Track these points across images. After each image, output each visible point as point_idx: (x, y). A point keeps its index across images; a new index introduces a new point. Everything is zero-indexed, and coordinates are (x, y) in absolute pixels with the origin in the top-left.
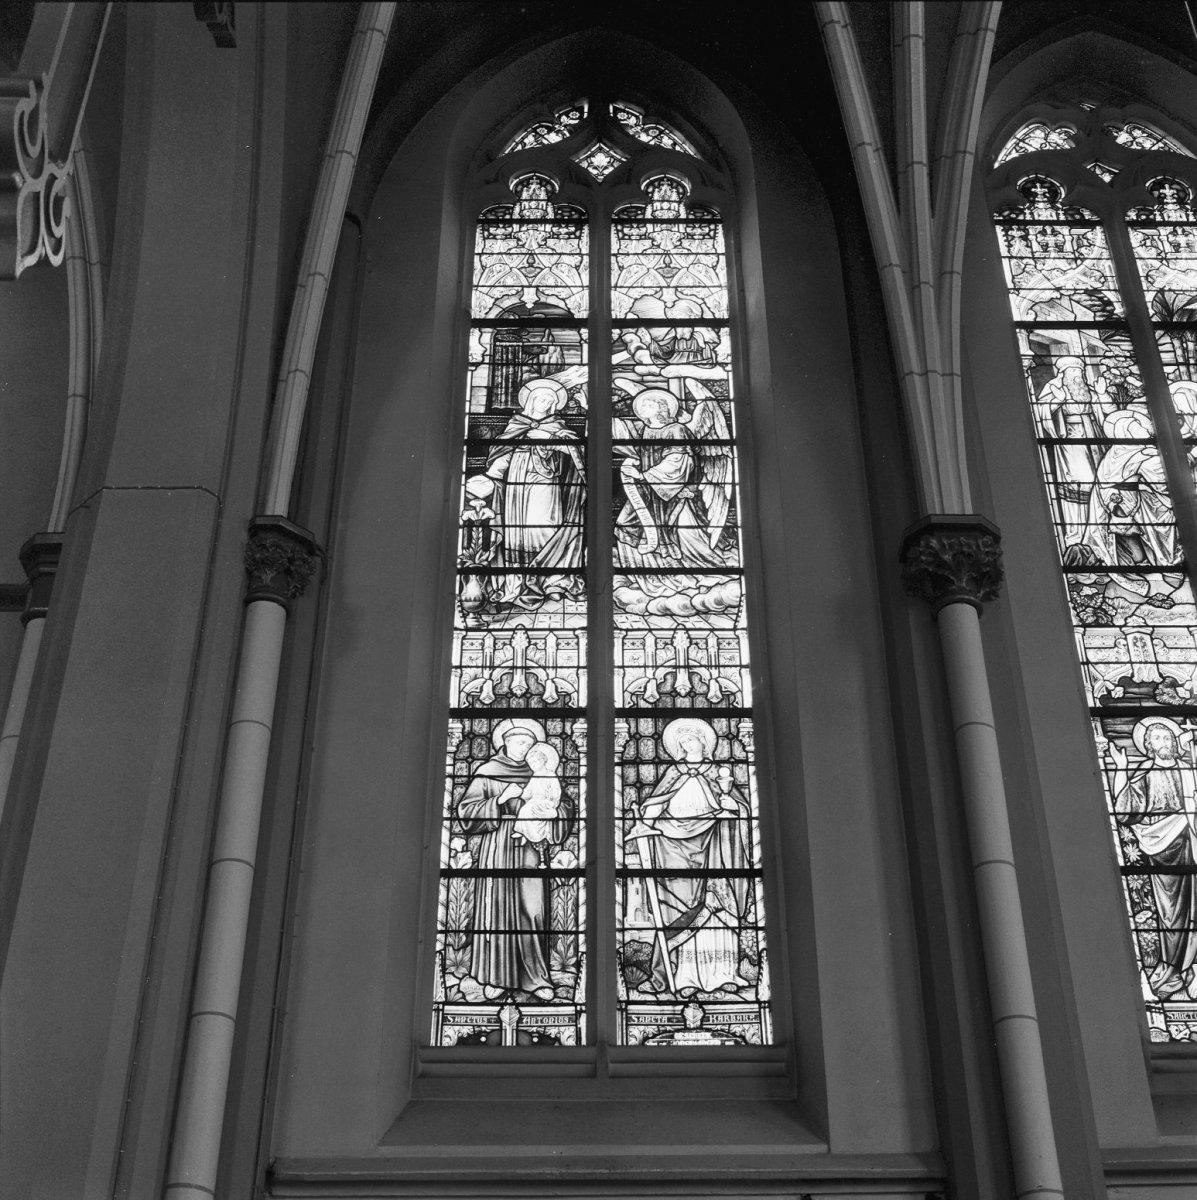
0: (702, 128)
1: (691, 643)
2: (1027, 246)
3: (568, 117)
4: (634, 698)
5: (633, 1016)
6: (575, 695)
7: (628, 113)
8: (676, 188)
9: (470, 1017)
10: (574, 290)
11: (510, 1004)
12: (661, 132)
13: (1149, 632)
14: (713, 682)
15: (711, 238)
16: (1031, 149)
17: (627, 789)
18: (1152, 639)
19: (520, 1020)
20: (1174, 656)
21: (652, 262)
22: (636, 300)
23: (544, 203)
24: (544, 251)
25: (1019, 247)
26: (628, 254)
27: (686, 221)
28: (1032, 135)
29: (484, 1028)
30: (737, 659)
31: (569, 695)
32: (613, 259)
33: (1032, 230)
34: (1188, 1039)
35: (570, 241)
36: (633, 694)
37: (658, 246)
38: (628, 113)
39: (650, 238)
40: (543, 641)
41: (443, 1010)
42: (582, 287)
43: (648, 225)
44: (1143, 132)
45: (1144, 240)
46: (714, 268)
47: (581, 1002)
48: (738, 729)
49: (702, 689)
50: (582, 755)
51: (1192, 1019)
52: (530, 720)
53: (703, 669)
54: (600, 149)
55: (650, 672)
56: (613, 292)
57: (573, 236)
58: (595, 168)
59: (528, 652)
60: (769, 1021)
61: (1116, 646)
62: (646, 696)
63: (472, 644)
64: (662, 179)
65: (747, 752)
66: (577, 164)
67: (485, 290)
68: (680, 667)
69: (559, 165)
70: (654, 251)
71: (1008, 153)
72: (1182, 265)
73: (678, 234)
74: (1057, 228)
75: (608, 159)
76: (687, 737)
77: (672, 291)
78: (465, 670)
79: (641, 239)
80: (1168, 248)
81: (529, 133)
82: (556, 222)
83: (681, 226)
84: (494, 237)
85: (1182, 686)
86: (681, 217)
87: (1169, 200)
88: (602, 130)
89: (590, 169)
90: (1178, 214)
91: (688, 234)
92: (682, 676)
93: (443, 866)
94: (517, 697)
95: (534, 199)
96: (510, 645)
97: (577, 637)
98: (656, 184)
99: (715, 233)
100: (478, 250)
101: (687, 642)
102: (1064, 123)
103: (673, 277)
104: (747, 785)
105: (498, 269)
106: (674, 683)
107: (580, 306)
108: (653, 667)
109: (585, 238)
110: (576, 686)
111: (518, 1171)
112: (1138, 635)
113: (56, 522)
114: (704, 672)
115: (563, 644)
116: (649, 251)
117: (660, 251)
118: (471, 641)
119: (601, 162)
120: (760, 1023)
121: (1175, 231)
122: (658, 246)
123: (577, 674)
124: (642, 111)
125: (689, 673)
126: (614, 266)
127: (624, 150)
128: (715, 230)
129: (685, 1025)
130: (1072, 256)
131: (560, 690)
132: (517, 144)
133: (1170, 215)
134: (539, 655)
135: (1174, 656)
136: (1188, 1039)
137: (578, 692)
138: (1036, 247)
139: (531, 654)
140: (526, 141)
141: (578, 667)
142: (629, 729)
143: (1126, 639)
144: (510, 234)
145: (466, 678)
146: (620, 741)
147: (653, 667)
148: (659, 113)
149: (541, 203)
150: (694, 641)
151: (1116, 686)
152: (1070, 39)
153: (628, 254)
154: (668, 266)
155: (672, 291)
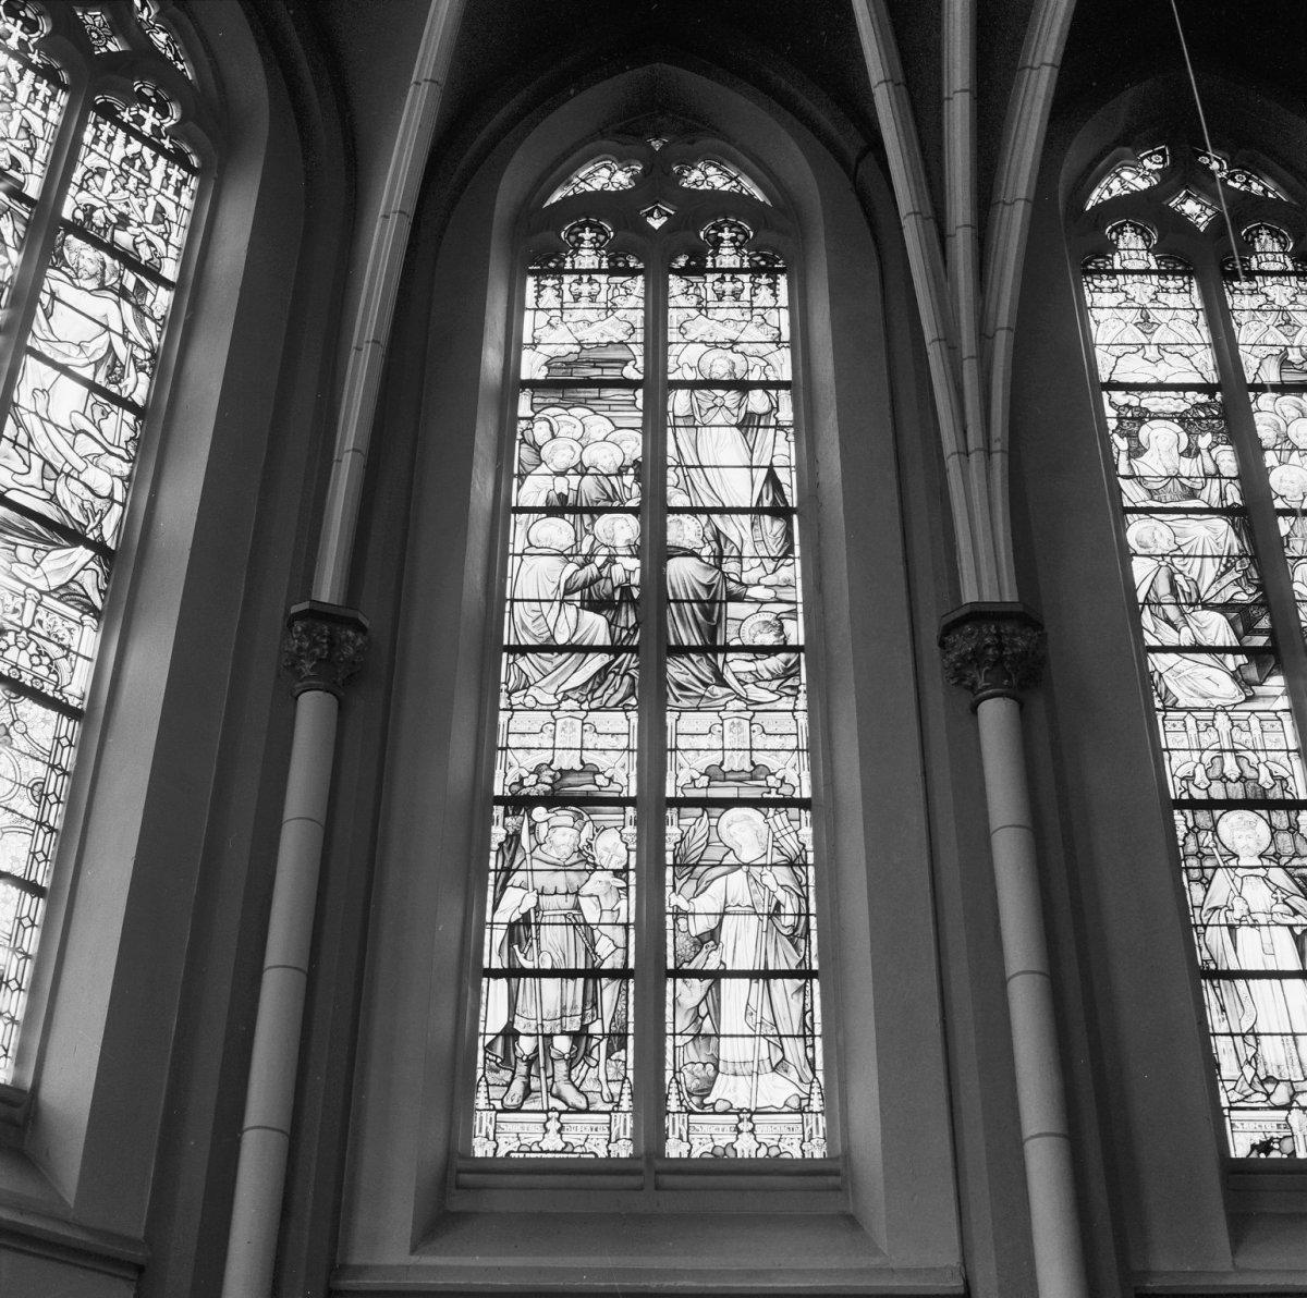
0: (770, 173)
2: (558, 296)
3: (1151, 161)
4: (1184, 783)
8: (1141, 235)
12: (1249, 177)
15: (1186, 292)
16: (589, 189)
18: (751, 725)
20: (603, 742)
22: (1118, 358)
23: (1145, 253)
24: (1156, 305)
25: (549, 298)
27: (1158, 273)
28: (596, 174)
33: (567, 279)
34: (712, 1153)
35: (1181, 295)
36: (1182, 779)
37: (1273, 302)
44: (719, 169)
45: (688, 287)
48: (1298, 823)
49: (1250, 773)
52: (751, 809)
53: (1250, 752)
55: (1196, 755)
57: (1182, 290)
61: (542, 731)
64: (1258, 228)
68: (1225, 751)
69: (1142, 210)
70: (1129, 305)
71: (1097, 196)
72: (721, 314)
74: (594, 276)
75: (1199, 207)
77: (1154, 348)
80: (711, 296)
83: (1153, 277)
84: (1101, 290)
90: (732, 259)
94: (1231, 781)
95: (1132, 249)
96: (1213, 726)
98: (1254, 232)
99: (1190, 287)
102: (610, 156)
110: (1289, 769)
111: (710, 1285)
112: (736, 720)
114: (1249, 754)
116: (1123, 305)
117: (1135, 305)
121: (581, 279)
122: (1133, 300)
124: (1227, 156)
125: (1236, 757)
128: (1190, 283)
130: (604, 306)
133: (724, 260)
134: (1246, 736)
135: (603, 742)
136: (712, 1153)
138: (567, 297)
139: (1236, 733)
140: (1111, 186)
142: (1186, 821)
144: (1117, 287)
149: (1277, 256)
152: (639, 71)
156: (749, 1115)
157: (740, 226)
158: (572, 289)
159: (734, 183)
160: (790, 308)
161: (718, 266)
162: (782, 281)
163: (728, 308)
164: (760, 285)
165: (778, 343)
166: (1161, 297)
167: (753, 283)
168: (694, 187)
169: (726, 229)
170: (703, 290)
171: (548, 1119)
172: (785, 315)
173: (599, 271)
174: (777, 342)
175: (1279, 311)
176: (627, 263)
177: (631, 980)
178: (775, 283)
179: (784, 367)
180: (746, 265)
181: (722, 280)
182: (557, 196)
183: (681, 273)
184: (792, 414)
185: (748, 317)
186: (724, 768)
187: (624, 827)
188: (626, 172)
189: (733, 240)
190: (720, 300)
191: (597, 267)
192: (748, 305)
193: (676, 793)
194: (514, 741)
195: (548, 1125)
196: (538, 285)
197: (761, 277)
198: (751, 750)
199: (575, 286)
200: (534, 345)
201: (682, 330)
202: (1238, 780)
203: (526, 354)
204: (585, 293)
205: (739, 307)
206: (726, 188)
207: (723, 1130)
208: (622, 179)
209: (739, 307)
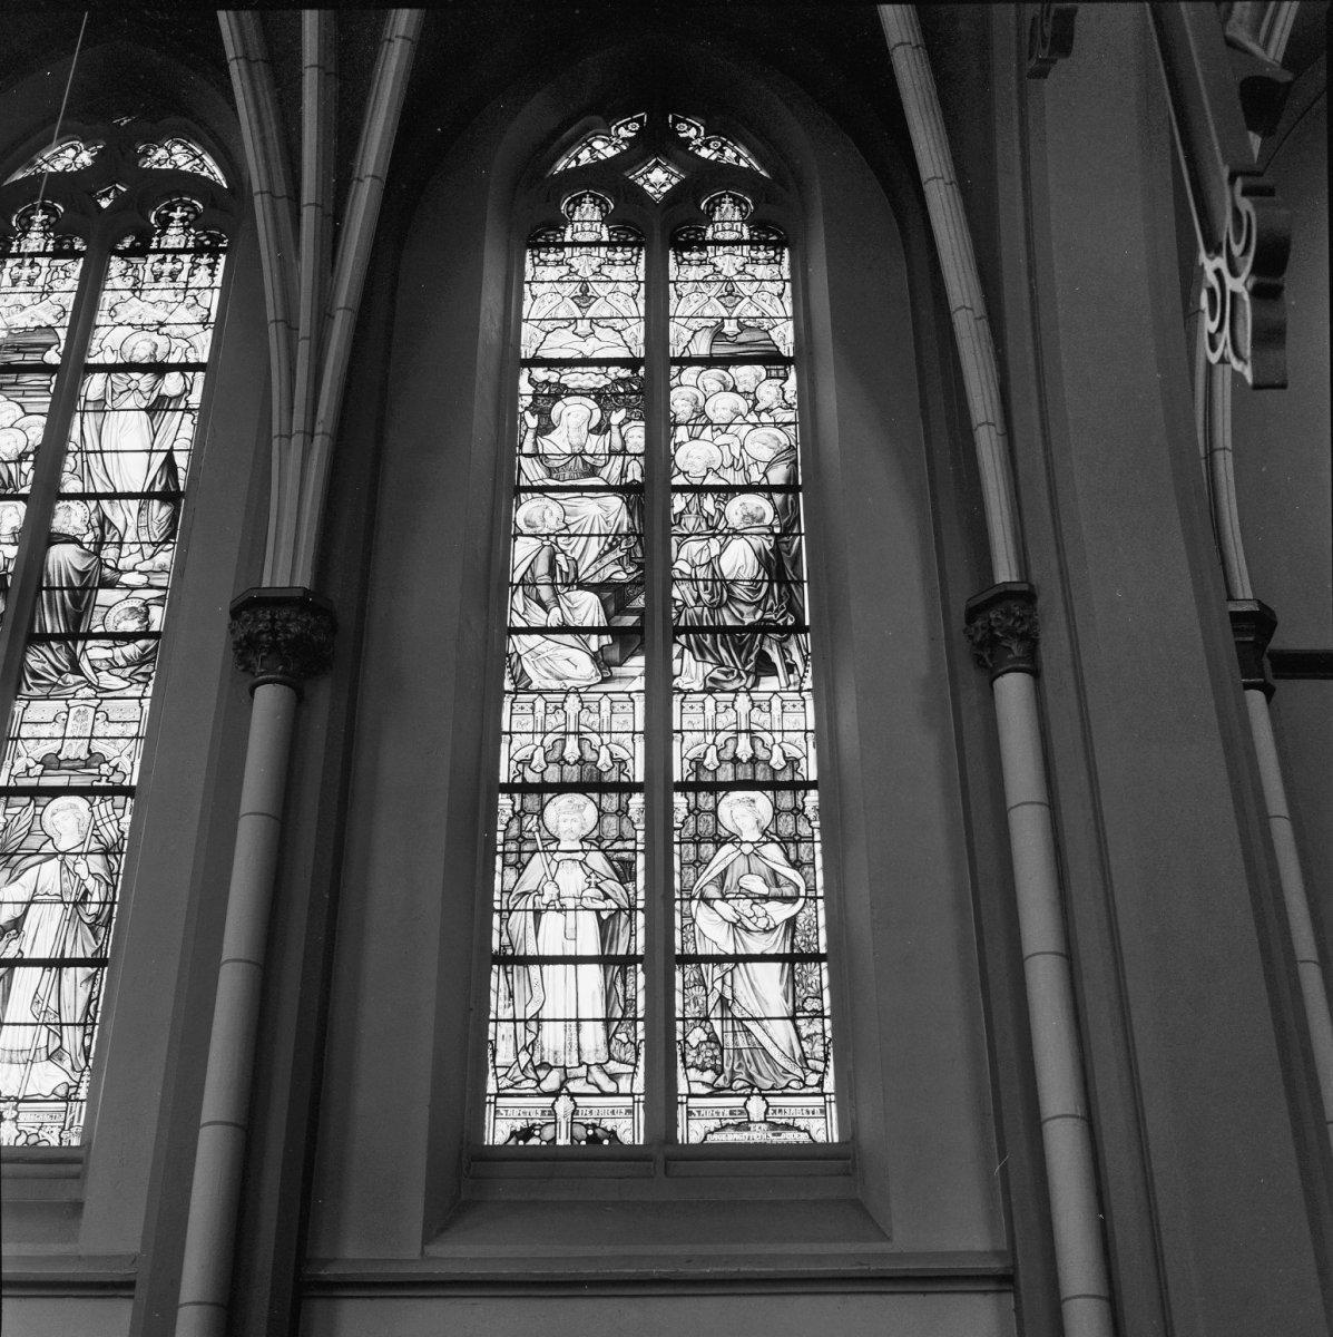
1: (753, 707)
3: (627, 129)
4: (520, 766)
5: (501, 1110)
6: (630, 762)
7: (688, 123)
9: (522, 1110)
10: (631, 321)
11: (756, 1095)
12: (724, 144)
13: (95, 705)
14: (776, 747)
17: (507, 869)
19: (574, 1112)
20: (114, 730)
21: (715, 289)
22: (695, 332)
23: (598, 225)
26: (542, 282)
27: (750, 242)
28: (61, 155)
29: (538, 1122)
30: (631, 724)
31: (798, 760)
32: (671, 286)
35: (626, 267)
37: (576, 273)
38: (688, 123)
39: (711, 264)
40: (767, 703)
41: (495, 1103)
42: (786, 318)
43: (566, 249)
46: (780, 296)
47: (638, 1092)
48: (803, 803)
50: (815, 831)
51: (811, 1115)
53: (595, 735)
54: (657, 164)
56: (524, 324)
57: (629, 262)
58: (652, 185)
59: (581, 715)
60: (834, 1115)
61: (54, 720)
62: (532, 766)
63: (692, 707)
65: (813, 828)
66: (632, 181)
67: (683, 321)
68: (741, 731)
70: (571, 278)
72: (154, 296)
73: (741, 258)
76: (67, 820)
77: (587, 322)
78: (516, 737)
79: (769, 263)
80: (149, 276)
81: (584, 148)
82: (610, 245)
83: (602, 249)
85: (108, 762)
86: (603, 240)
87: (36, 227)
88: (656, 143)
89: (646, 187)
91: (752, 259)
92: (572, 742)
93: (678, 952)
95: (587, 220)
96: (562, 708)
97: (804, 699)
100: (528, 278)
101: (579, 706)
103: (589, 306)
104: (812, 864)
105: (550, 298)
106: (563, 752)
107: (636, 339)
108: (712, 731)
109: (642, 264)
113: (1005, 571)
115: (526, 708)
118: (520, 705)
119: (658, 180)
120: (826, 1118)
121: (23, 263)
122: (576, 273)
123: (633, 740)
125: (751, 738)
126: (527, 295)
127: (682, 168)
128: (638, 254)
129: (748, 1118)
131: (615, 757)
132: (571, 160)
134: (594, 718)
135: (114, 730)
137: (633, 759)
140: (580, 156)
141: (634, 733)
142: (513, 805)
143: (68, 713)
145: (516, 744)
146: (503, 818)
147: (712, 731)
148: (719, 129)
150: (757, 704)
151: (37, 763)
153: (542, 282)
154: (730, 294)
155: (587, 322)
158: (154, 269)
164: (200, 265)
176: (72, 245)
181: (20, 266)
188: (92, 152)
198: (91, 738)
201: (113, 313)
202: (576, 762)
204: (25, 277)
206: (187, 168)
207: (813, 1113)
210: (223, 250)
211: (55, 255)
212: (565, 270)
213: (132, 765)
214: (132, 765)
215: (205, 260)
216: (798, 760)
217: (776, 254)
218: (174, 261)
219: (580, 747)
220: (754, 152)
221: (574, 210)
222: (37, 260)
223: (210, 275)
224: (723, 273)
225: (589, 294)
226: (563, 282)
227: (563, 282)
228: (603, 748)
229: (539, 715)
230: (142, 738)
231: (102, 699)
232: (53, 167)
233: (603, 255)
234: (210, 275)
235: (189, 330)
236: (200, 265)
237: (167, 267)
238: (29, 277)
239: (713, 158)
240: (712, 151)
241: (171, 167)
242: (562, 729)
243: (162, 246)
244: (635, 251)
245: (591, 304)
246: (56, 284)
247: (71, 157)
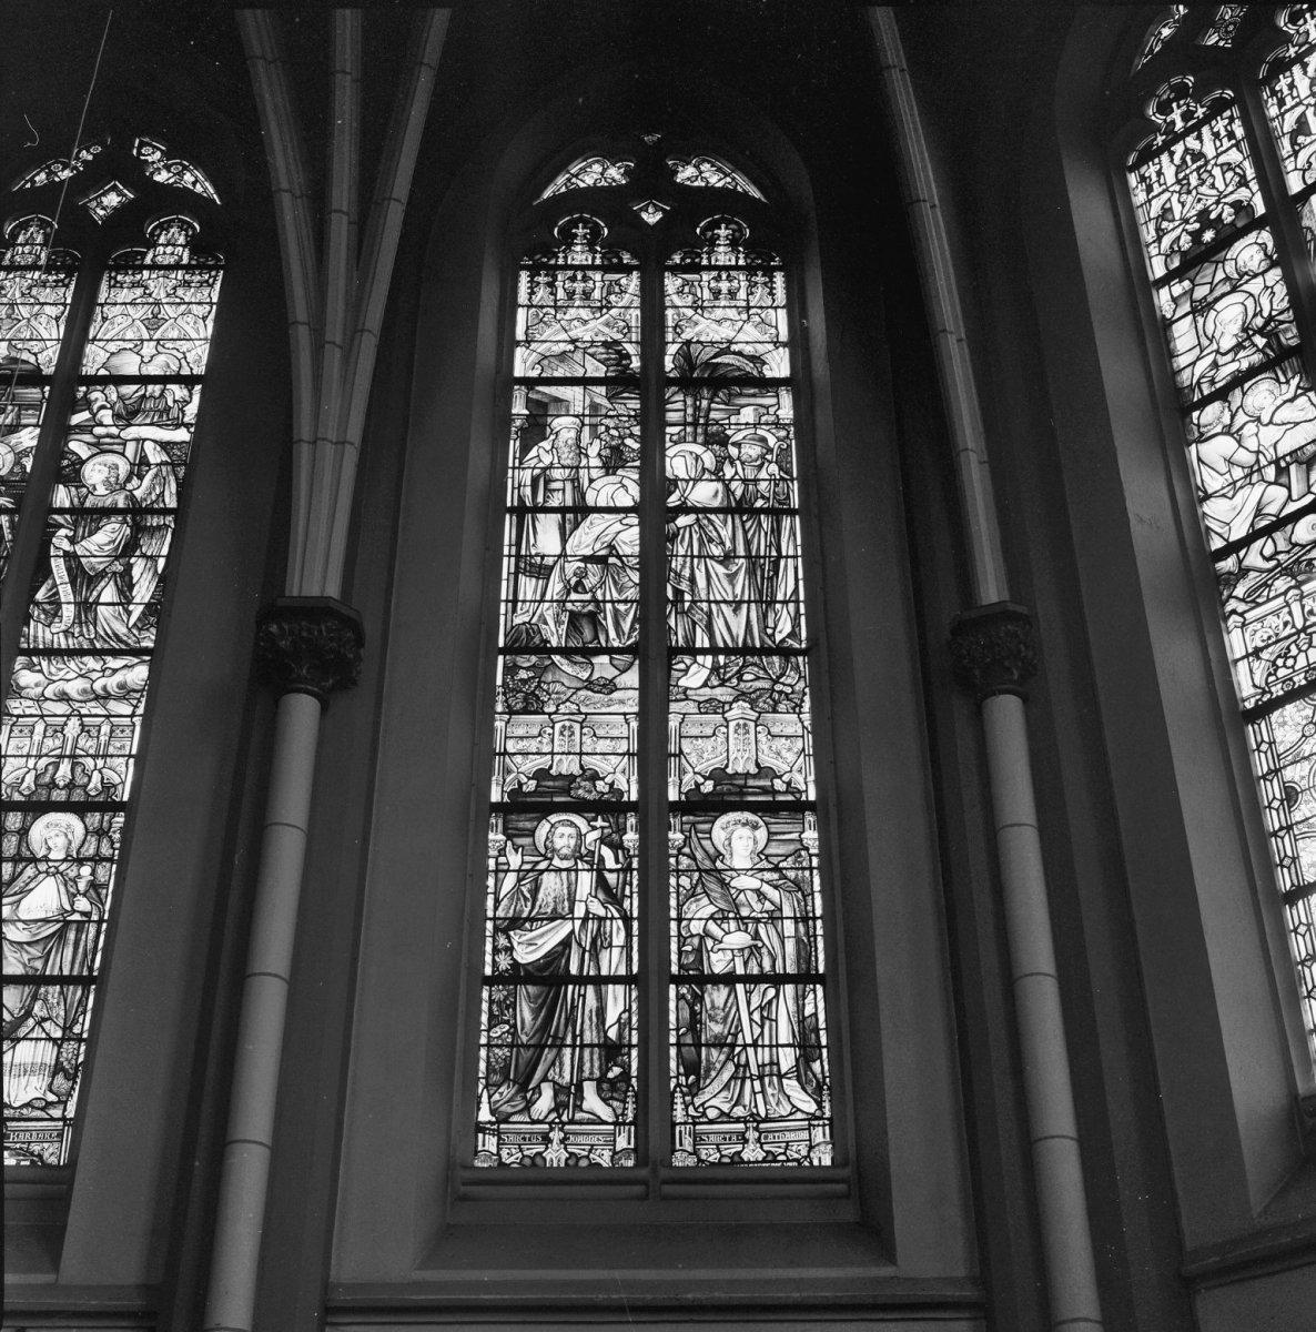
1: (82, 731)
2: (551, 294)
10: (197, 343)
12: (185, 168)
13: (580, 720)
16: (582, 185)
20: (602, 746)
22: (112, 354)
25: (542, 294)
37: (150, 295)
40: (97, 728)
61: (714, 734)
72: (719, 313)
73: (174, 281)
77: (153, 344)
80: (707, 294)
82: (188, 268)
83: (180, 272)
92: (65, 767)
96: (62, 732)
109: (72, 287)
112: (567, 724)
118: (20, 728)
121: (720, 276)
128: (215, 277)
132: (27, 182)
135: (602, 746)
138: (561, 294)
140: (37, 179)
155: (153, 344)
156: (755, 1124)
157: (736, 223)
158: (566, 286)
159: (729, 180)
160: (789, 307)
161: (713, 263)
162: (779, 279)
163: (724, 307)
164: (757, 283)
165: (775, 343)
166: (180, 292)
167: (749, 281)
168: (688, 183)
169: (580, 225)
170: (699, 290)
171: (747, 1129)
172: (782, 314)
173: (593, 267)
174: (776, 343)
175: (156, 304)
176: (621, 259)
177: (93, 987)
178: (772, 282)
179: (782, 365)
180: (598, 262)
181: (573, 279)
182: (547, 194)
183: (676, 270)
184: (792, 412)
185: (744, 317)
186: (729, 771)
187: (803, 832)
188: (619, 168)
189: (584, 236)
190: (717, 298)
191: (590, 262)
192: (744, 304)
193: (502, 798)
194: (511, 746)
195: (747, 1135)
196: (531, 281)
197: (757, 275)
198: (581, 754)
199: (713, 284)
200: (528, 342)
201: (678, 330)
202: (66, 786)
203: (519, 352)
204: (725, 291)
205: (735, 307)
206: (720, 185)
207: (730, 1139)
208: (615, 174)
209: (735, 307)
210: (222, 267)
211: (605, 269)
212: (139, 291)
213: (628, 782)
214: (628, 782)
215: (760, 279)
216: (115, 786)
217: (210, 277)
218: (585, 279)
219: (73, 770)
220: (210, 177)
221: (160, 234)
222: (590, 273)
223: (769, 294)
224: (154, 295)
225: (159, 316)
226: (135, 304)
227: (135, 304)
228: (96, 773)
229: (37, 737)
230: (633, 754)
231: (586, 714)
232: (584, 182)
233: (180, 277)
234: (769, 294)
235: (761, 349)
236: (757, 283)
237: (579, 286)
238: (729, 291)
239: (171, 181)
240: (171, 175)
241: (703, 184)
242: (58, 752)
243: (569, 262)
244: (213, 273)
245: (159, 327)
246: (612, 298)
247: (594, 174)
